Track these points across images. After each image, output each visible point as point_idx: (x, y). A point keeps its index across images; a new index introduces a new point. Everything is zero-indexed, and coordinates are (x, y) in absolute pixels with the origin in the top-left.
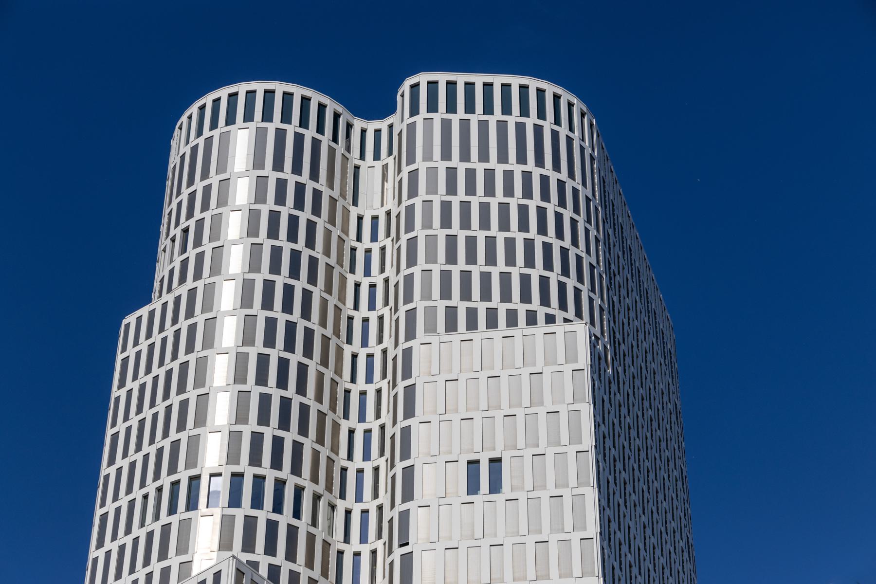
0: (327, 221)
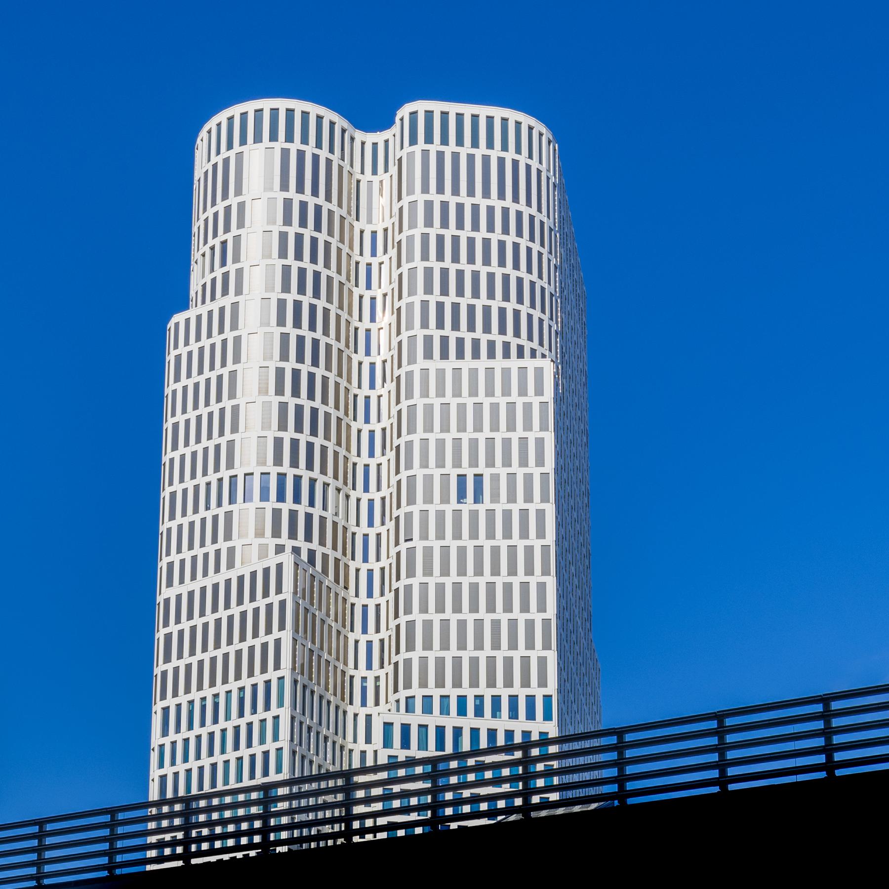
0: (339, 240)
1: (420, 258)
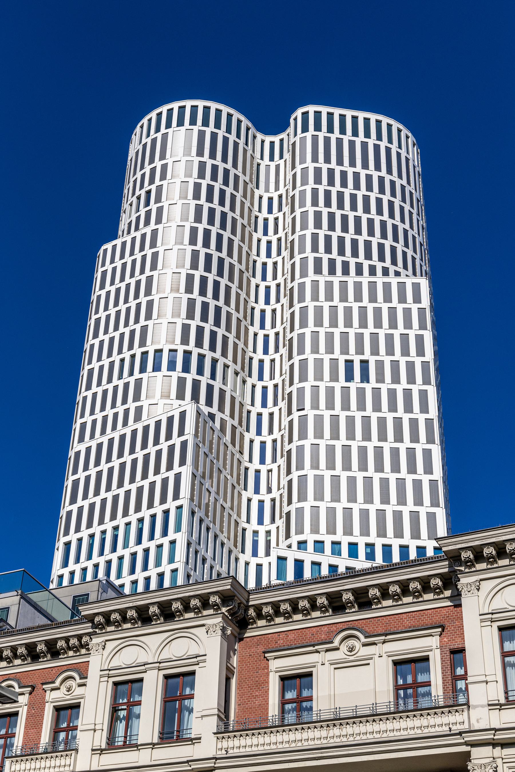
0: (242, 196)
1: (309, 532)
